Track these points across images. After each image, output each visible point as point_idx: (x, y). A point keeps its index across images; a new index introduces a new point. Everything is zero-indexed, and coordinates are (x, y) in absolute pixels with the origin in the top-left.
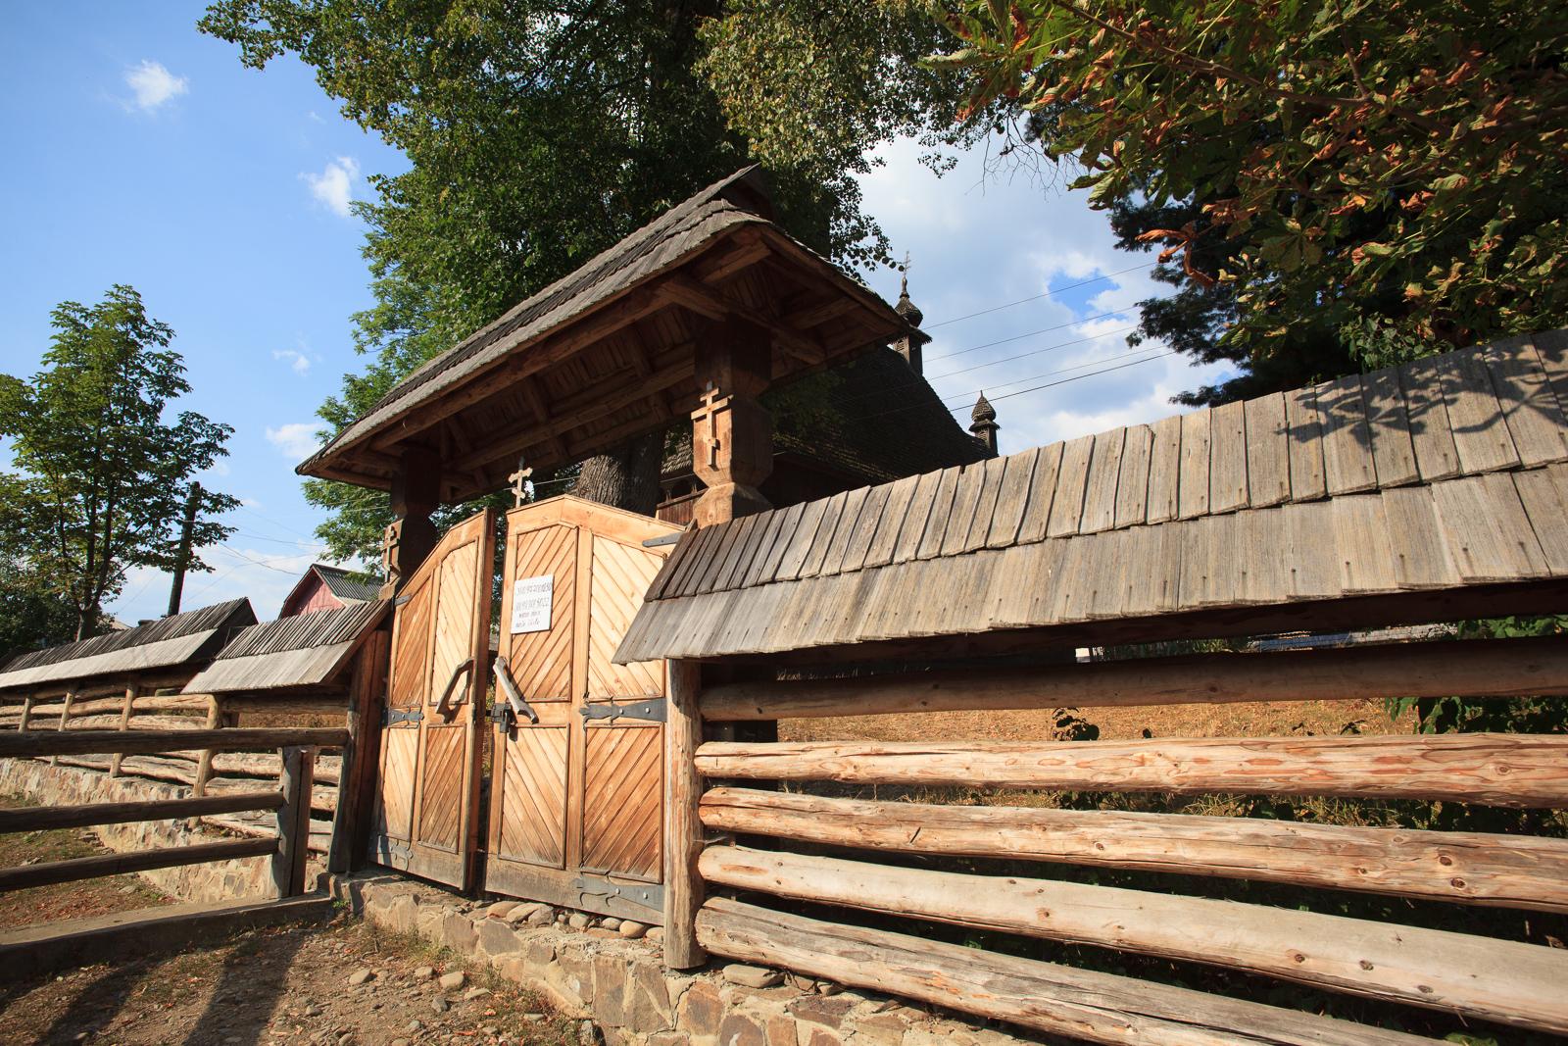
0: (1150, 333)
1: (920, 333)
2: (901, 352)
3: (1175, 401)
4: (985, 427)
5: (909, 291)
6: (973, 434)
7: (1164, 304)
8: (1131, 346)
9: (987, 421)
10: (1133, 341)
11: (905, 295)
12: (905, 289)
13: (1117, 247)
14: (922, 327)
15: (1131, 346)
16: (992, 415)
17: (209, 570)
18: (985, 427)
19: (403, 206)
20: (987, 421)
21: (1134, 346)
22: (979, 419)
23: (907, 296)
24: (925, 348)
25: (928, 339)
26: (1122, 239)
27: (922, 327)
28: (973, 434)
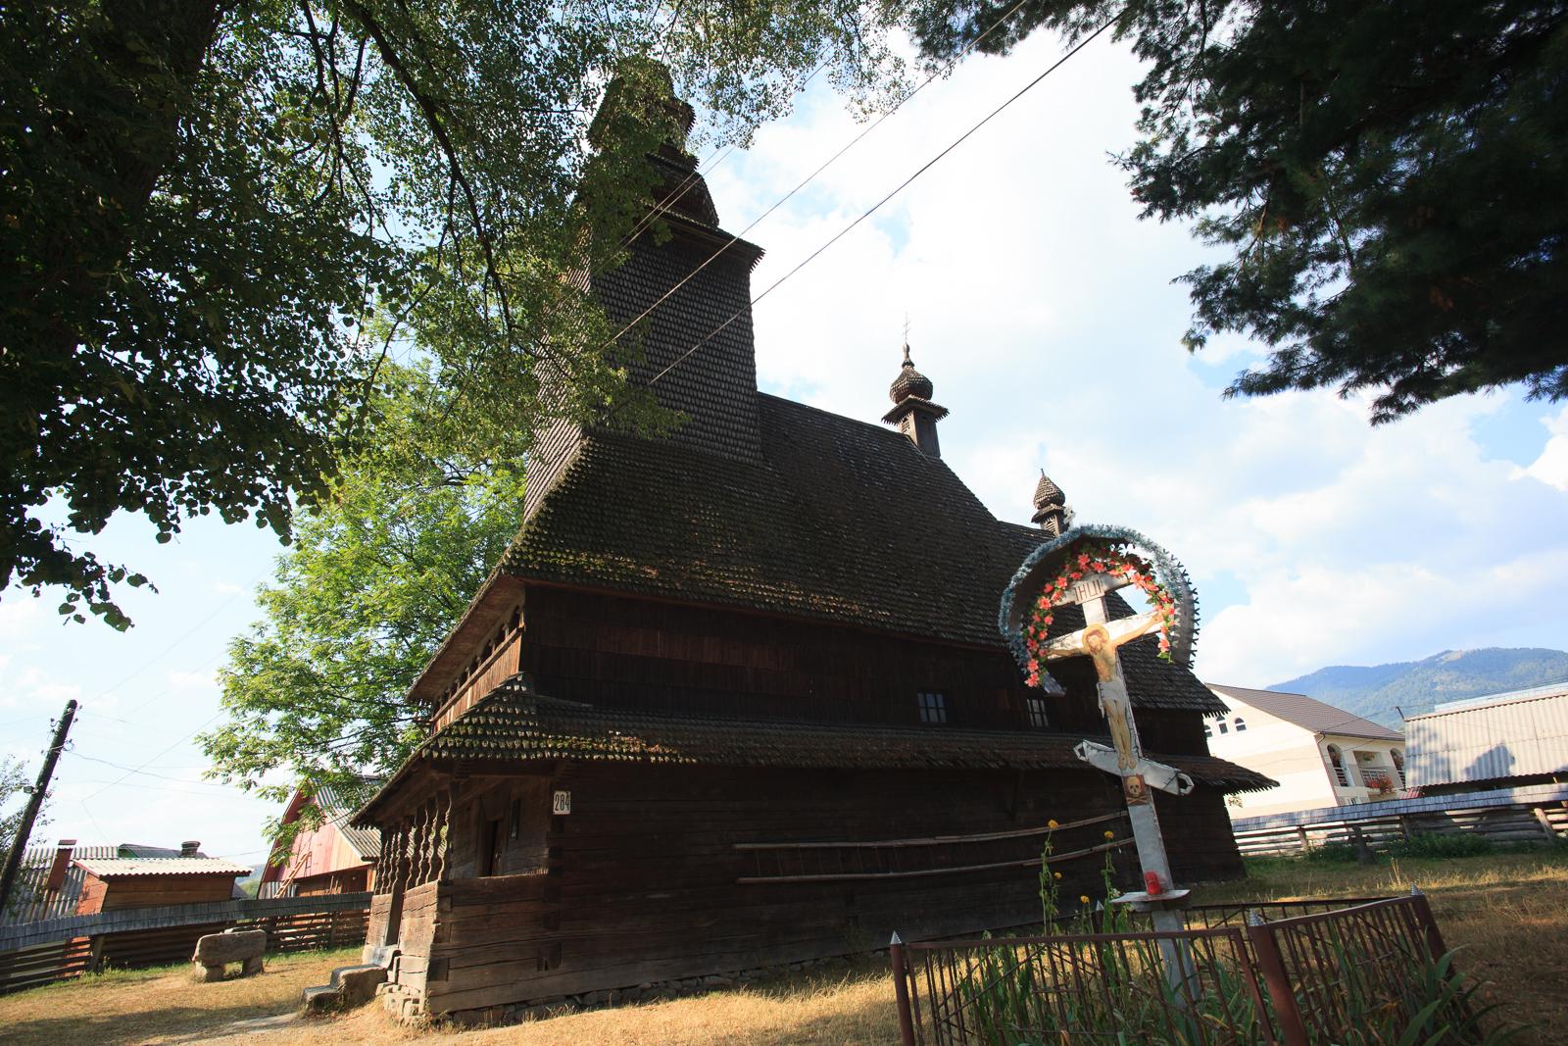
0: (1217, 325)
1: (933, 406)
2: (907, 433)
3: (1231, 392)
4: (1051, 514)
5: (913, 358)
6: (1037, 526)
7: (1221, 274)
8: (1192, 349)
9: (1053, 506)
10: (1195, 342)
11: (908, 363)
12: (908, 356)
13: (1141, 217)
14: (935, 400)
15: (1192, 349)
16: (1059, 498)
17: (156, 591)
18: (1051, 514)
19: (364, 139)
20: (1053, 506)
21: (1197, 348)
22: (1042, 505)
23: (911, 364)
24: (941, 425)
25: (942, 412)
26: (1146, 205)
27: (935, 400)
28: (1037, 526)
